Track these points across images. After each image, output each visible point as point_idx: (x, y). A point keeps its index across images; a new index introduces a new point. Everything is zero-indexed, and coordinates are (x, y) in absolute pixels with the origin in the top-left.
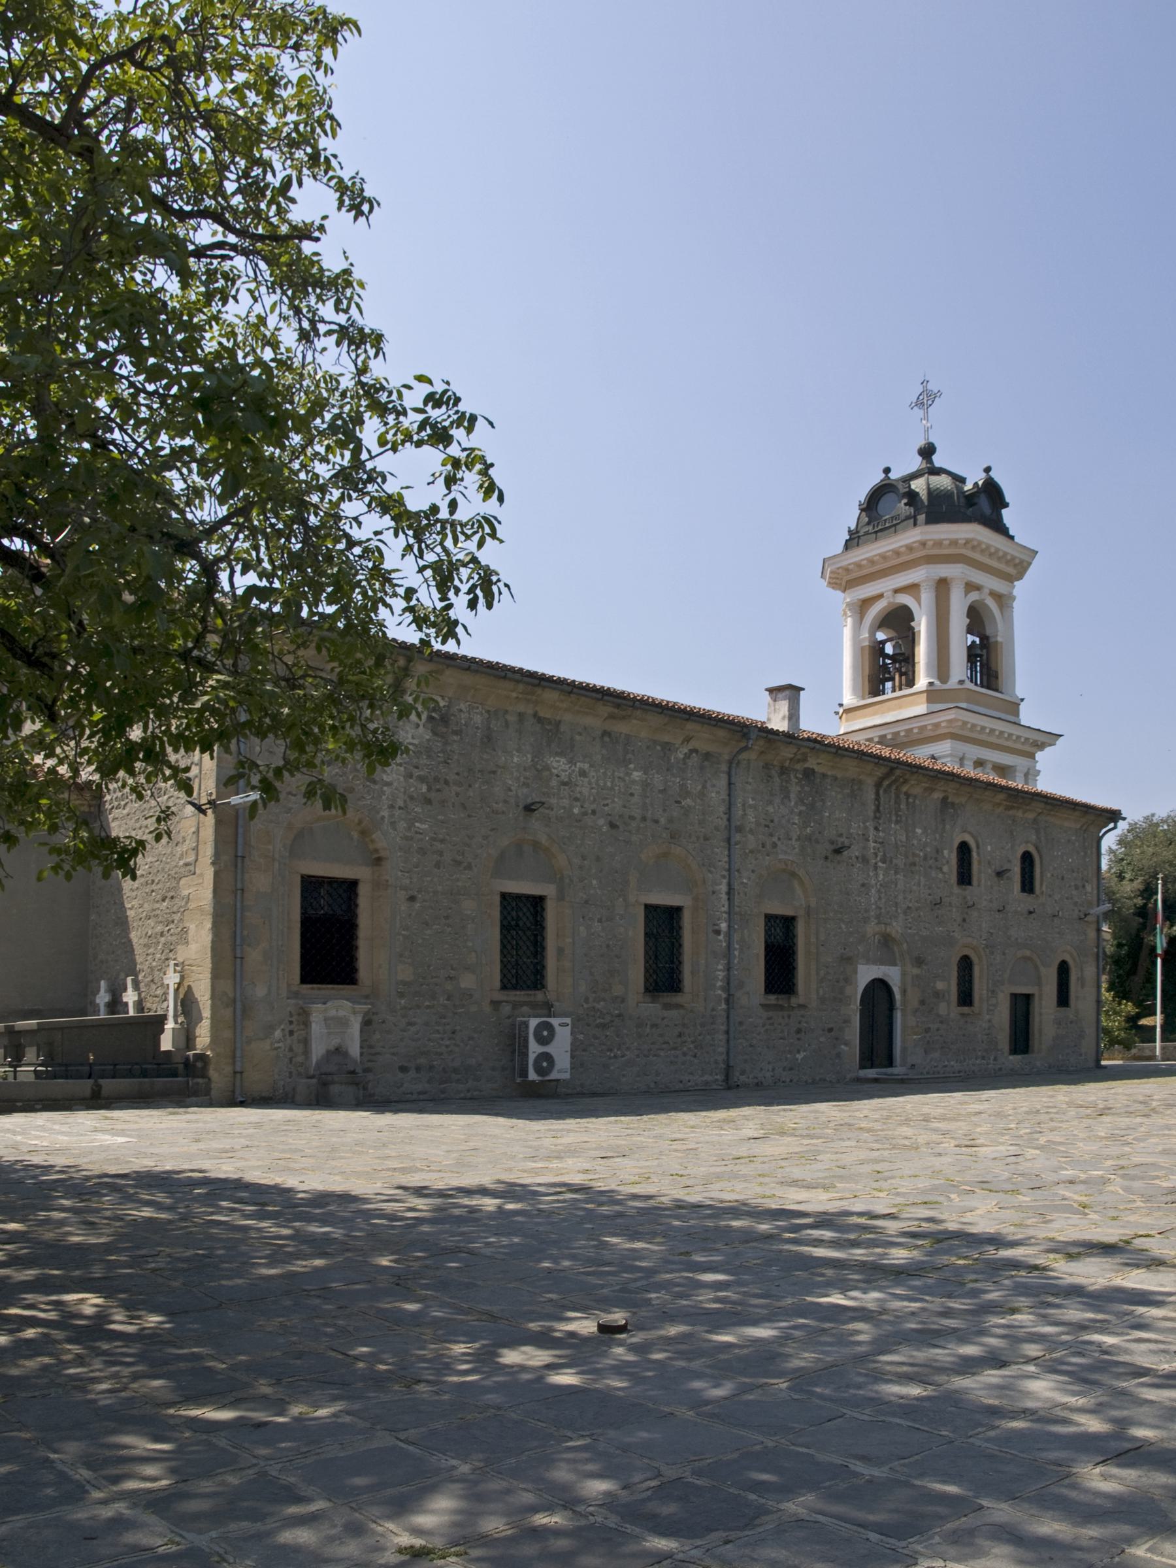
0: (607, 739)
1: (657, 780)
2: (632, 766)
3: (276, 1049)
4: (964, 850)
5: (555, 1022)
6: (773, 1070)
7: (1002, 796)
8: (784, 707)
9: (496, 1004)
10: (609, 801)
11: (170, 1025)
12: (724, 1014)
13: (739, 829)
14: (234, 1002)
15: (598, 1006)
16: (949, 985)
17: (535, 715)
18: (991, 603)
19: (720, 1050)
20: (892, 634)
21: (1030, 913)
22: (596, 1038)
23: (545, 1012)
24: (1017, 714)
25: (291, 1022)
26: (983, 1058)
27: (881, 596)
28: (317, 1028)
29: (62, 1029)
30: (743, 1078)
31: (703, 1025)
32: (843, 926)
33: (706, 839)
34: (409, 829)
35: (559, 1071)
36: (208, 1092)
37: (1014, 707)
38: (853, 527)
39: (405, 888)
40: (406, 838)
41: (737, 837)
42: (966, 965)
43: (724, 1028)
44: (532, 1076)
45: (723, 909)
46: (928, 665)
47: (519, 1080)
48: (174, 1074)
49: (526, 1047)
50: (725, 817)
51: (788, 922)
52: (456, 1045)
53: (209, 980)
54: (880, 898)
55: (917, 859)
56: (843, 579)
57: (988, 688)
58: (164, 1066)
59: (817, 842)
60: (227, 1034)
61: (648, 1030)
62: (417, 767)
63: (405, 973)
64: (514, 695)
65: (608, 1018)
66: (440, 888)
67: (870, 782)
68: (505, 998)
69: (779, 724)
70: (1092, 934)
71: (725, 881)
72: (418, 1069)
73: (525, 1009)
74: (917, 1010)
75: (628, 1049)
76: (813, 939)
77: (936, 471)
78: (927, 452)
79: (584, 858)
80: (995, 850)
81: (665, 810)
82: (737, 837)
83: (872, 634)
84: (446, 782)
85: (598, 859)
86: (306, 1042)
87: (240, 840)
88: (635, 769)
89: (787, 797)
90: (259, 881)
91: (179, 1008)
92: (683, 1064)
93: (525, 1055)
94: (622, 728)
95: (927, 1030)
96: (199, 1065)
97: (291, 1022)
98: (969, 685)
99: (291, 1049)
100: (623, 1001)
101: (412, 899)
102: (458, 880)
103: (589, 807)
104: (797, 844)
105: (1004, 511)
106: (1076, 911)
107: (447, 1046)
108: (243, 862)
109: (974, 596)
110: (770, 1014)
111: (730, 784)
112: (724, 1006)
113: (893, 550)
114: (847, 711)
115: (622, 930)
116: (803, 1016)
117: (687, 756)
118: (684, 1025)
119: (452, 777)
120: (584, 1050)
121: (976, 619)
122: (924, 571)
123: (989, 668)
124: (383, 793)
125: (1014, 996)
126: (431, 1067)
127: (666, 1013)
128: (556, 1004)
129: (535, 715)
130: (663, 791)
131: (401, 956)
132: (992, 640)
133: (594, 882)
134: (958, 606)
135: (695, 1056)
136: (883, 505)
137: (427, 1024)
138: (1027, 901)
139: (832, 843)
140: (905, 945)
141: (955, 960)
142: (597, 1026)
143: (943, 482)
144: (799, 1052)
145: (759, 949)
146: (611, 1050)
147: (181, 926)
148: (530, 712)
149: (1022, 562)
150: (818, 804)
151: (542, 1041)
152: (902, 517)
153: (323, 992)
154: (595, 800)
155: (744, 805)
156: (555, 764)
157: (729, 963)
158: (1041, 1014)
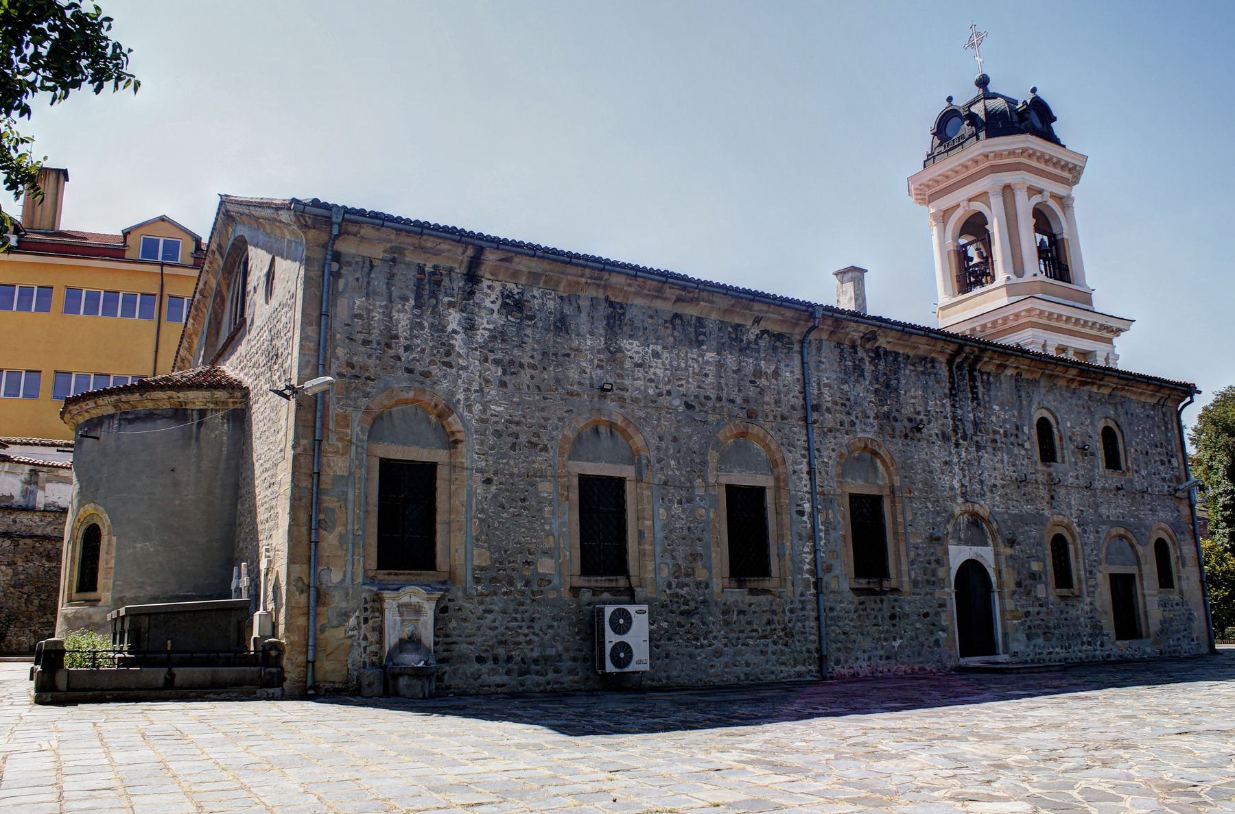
1: (731, 360)
2: (704, 347)
3: (351, 637)
4: (1044, 427)
5: (632, 609)
6: (869, 659)
8: (849, 288)
9: (575, 590)
10: (683, 382)
13: (816, 408)
14: (310, 591)
16: (1043, 564)
17: (607, 299)
19: (812, 638)
20: (972, 238)
25: (366, 609)
26: (1089, 644)
27: (958, 206)
28: (391, 616)
29: (149, 615)
31: (792, 611)
32: (930, 505)
33: (783, 418)
34: (484, 411)
37: (1086, 297)
40: (482, 421)
42: (1059, 545)
43: (814, 614)
45: (805, 489)
46: (1004, 261)
47: (600, 672)
50: (801, 396)
52: (534, 634)
54: (964, 476)
55: (997, 437)
59: (896, 419)
61: (735, 617)
62: (492, 351)
63: (482, 557)
64: (583, 280)
65: (693, 605)
66: (516, 471)
67: (942, 359)
68: (586, 584)
69: (847, 304)
70: (1185, 511)
71: (805, 460)
72: (496, 659)
73: (606, 596)
74: (1014, 593)
75: (715, 638)
76: (900, 519)
77: (995, 96)
78: (983, 82)
79: (661, 439)
81: (740, 390)
82: (815, 416)
83: (955, 240)
84: (521, 366)
86: (380, 630)
87: (318, 425)
88: (707, 350)
89: (862, 375)
90: (336, 465)
92: (774, 653)
94: (691, 311)
96: (273, 653)
97: (366, 609)
99: (365, 638)
100: (707, 586)
101: (488, 481)
104: (875, 423)
105: (1053, 125)
106: (1166, 488)
107: (526, 635)
108: (320, 445)
109: (1037, 199)
110: (862, 598)
111: (803, 363)
112: (813, 591)
113: (962, 165)
114: (943, 309)
115: (703, 511)
116: (896, 600)
117: (759, 337)
118: (774, 612)
119: (526, 360)
120: (669, 639)
121: (1042, 220)
122: (993, 178)
124: (459, 376)
125: (1114, 578)
126: (509, 659)
127: (753, 599)
128: (638, 590)
129: (607, 299)
131: (478, 540)
132: (1059, 237)
133: (672, 463)
134: (1024, 206)
135: (786, 645)
136: (949, 127)
137: (504, 612)
138: (1114, 479)
139: (910, 420)
140: (995, 524)
142: (682, 613)
143: (999, 104)
144: (895, 639)
146: (697, 639)
148: (601, 296)
149: (1075, 166)
150: (894, 382)
151: (619, 630)
153: (400, 577)
154: (669, 381)
155: (819, 384)
156: (629, 347)
157: (814, 546)
158: (1144, 595)
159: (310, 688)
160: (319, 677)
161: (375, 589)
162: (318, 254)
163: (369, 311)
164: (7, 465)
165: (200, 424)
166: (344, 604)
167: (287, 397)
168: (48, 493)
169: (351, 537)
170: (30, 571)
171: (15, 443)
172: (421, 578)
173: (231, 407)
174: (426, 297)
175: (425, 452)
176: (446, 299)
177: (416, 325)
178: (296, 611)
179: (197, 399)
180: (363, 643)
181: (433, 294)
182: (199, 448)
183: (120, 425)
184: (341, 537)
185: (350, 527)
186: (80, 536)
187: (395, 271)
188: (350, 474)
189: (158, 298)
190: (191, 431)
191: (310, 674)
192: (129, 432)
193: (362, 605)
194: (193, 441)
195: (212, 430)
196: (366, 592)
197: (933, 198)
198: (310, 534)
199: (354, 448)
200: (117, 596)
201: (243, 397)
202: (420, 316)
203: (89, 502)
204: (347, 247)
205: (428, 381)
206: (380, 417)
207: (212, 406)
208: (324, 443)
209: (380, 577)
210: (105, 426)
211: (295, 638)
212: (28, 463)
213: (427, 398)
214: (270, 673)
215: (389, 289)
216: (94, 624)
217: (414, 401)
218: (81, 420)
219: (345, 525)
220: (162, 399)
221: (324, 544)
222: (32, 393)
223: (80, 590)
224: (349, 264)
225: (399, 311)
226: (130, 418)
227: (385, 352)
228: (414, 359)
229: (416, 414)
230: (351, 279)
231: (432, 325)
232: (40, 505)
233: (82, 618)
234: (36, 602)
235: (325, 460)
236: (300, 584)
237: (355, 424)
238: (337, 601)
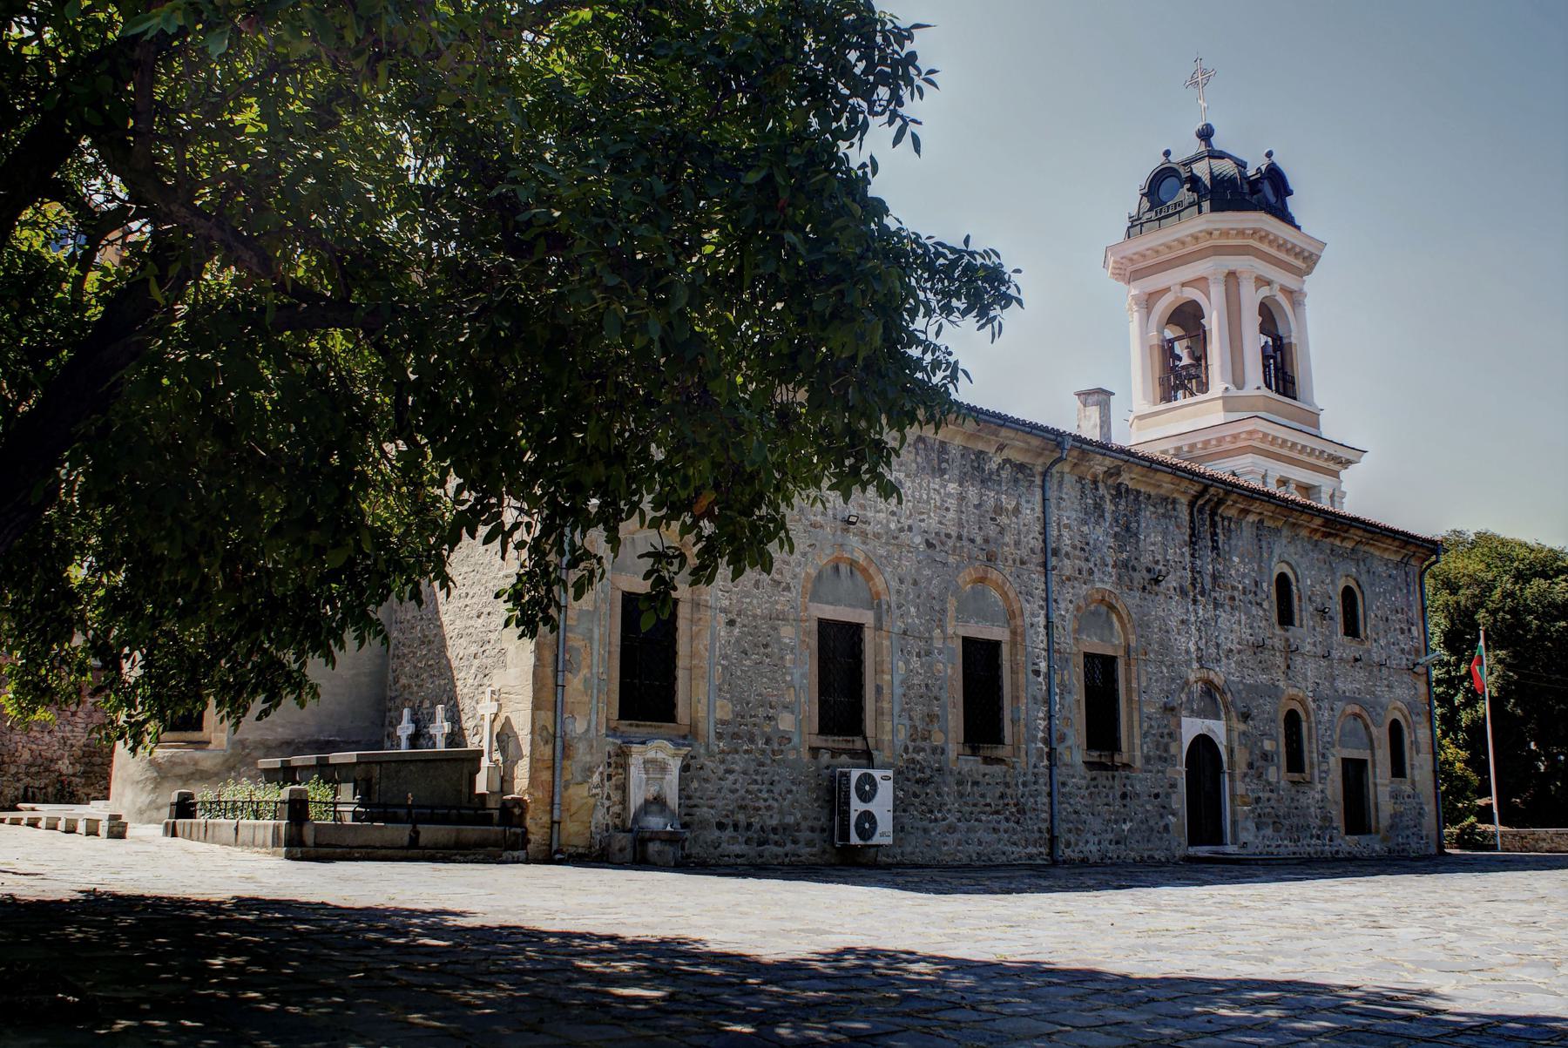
0: (921, 446)
1: (972, 493)
4: (1283, 583)
7: (1318, 521)
8: (1094, 413)
9: (815, 751)
11: (485, 762)
12: (1047, 771)
14: (555, 743)
15: (919, 757)
16: (1275, 744)
18: (1281, 298)
19: (1044, 815)
21: (1356, 660)
22: (916, 795)
23: (864, 762)
24: (1316, 425)
25: (609, 765)
26: (1318, 837)
27: (1168, 289)
28: (636, 773)
29: (380, 763)
30: (1068, 852)
31: (1025, 784)
33: (1023, 563)
35: (882, 835)
36: (521, 842)
38: (1134, 213)
39: (724, 611)
41: (1053, 561)
42: (1292, 720)
44: (855, 840)
48: (487, 820)
49: (848, 804)
50: (1040, 538)
51: (1108, 663)
53: (529, 712)
56: (1132, 271)
57: (1285, 394)
58: (472, 809)
59: (1134, 569)
60: (546, 776)
65: (928, 772)
66: (759, 611)
69: (1091, 432)
73: (844, 758)
76: (1134, 685)
78: (1206, 134)
79: (901, 581)
80: (1318, 582)
82: (1053, 561)
83: (1161, 331)
85: (915, 583)
86: (623, 788)
91: (495, 744)
93: (845, 814)
95: (1258, 800)
96: (517, 811)
98: (1265, 391)
99: (609, 797)
101: (731, 623)
102: (777, 602)
103: (906, 523)
109: (1265, 291)
112: (1046, 762)
114: (1140, 418)
115: (940, 667)
117: (1001, 467)
118: (1007, 785)
121: (1269, 318)
122: (1210, 258)
123: (1285, 373)
126: (749, 826)
130: (977, 507)
132: (1285, 341)
134: (1251, 298)
136: (1165, 189)
137: (745, 773)
139: (1149, 570)
141: (1281, 716)
142: (917, 782)
143: (1226, 168)
145: (1078, 694)
146: (931, 812)
147: (498, 647)
150: (1134, 525)
152: (1186, 203)
153: (641, 729)
157: (1049, 711)
158: (1375, 785)
160: (563, 841)
161: (619, 742)
166: (588, 758)
180: (607, 803)
185: (595, 670)
196: (611, 744)
197: (1136, 276)
198: (556, 676)
209: (622, 728)
211: (539, 794)
219: (590, 667)
233: (183, 764)
238: (582, 754)
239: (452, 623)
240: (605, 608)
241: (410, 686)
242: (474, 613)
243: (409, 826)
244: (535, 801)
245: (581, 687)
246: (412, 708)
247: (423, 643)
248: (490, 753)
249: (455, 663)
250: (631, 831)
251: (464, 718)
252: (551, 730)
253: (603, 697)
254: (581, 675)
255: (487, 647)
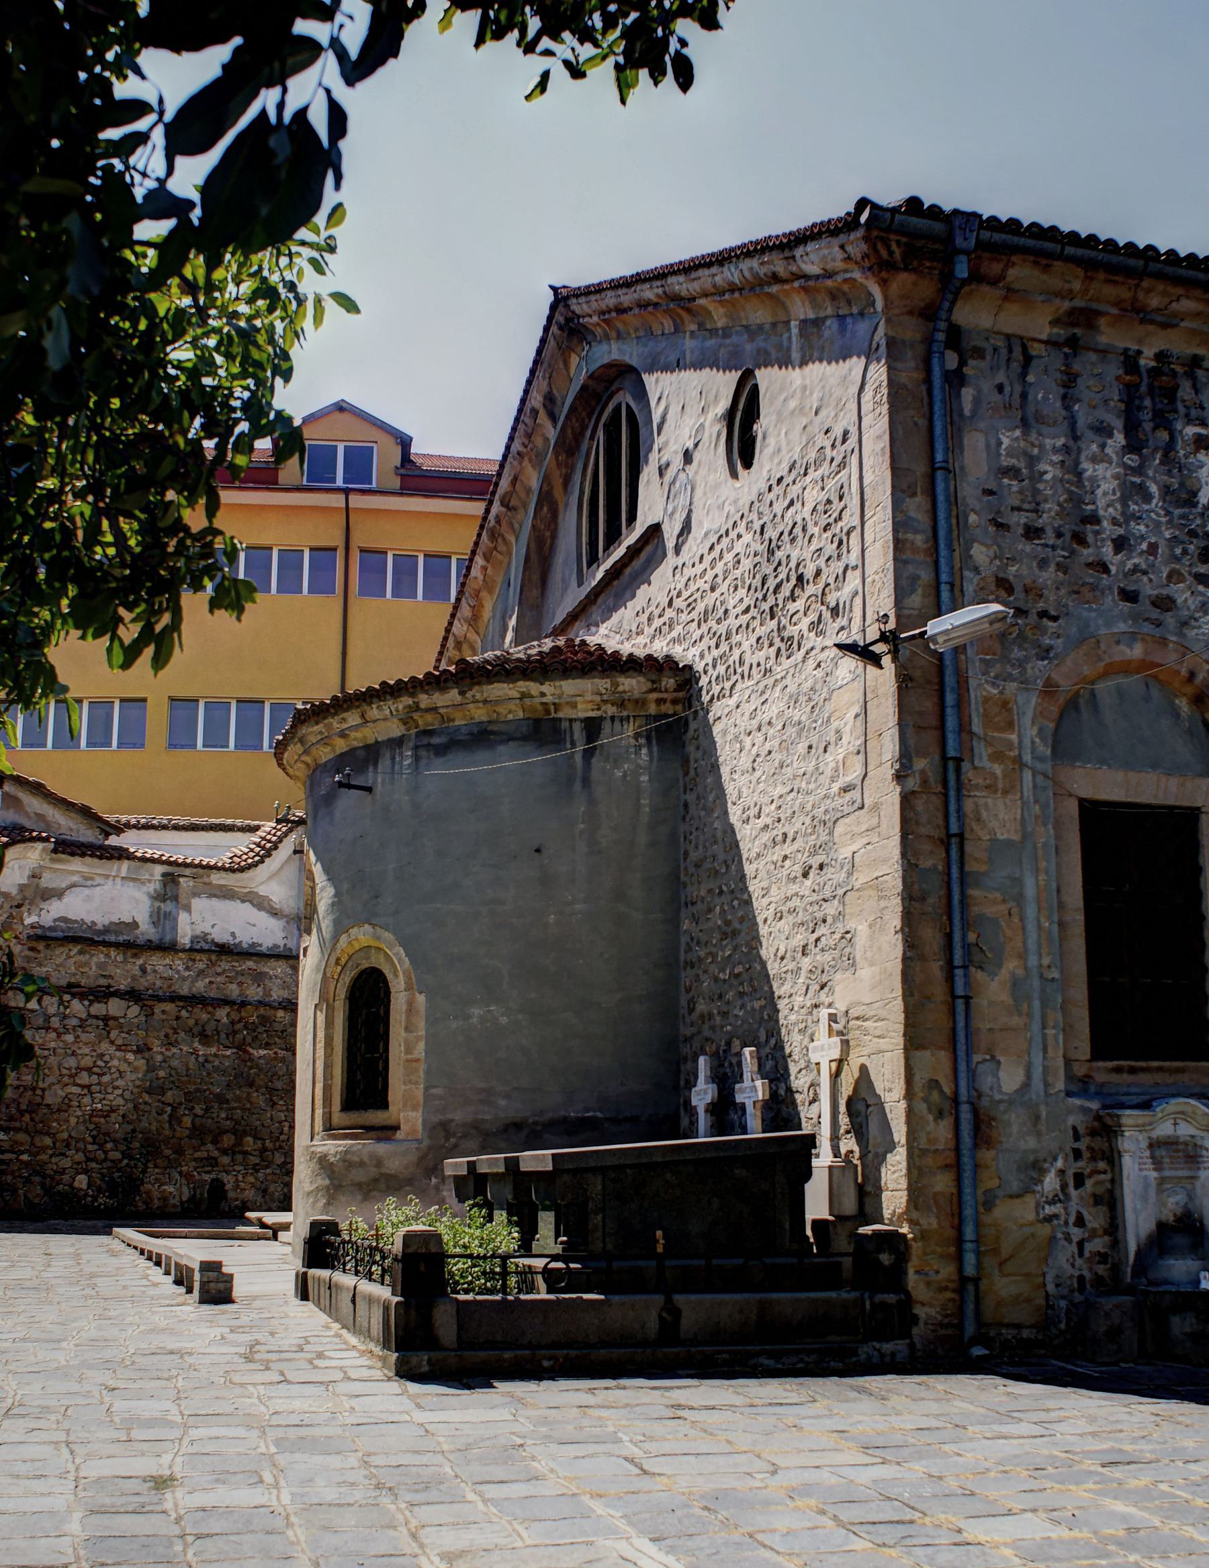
3: (1049, 1219)
11: (823, 1159)
14: (959, 1118)
25: (1077, 1154)
29: (602, 1170)
36: (902, 1317)
53: (899, 1054)
60: (942, 1183)
86: (1110, 1201)
87: (951, 722)
90: (997, 816)
91: (844, 1120)
96: (885, 1258)
99: (1080, 1222)
108: (958, 771)
147: (840, 928)
153: (1142, 1078)
159: (974, 1341)
160: (988, 1315)
161: (1094, 1105)
162: (912, 331)
163: (1032, 461)
164: (125, 865)
165: (588, 754)
166: (1031, 1143)
167: (875, 660)
168: (196, 916)
169: (1036, 983)
170: (175, 1063)
171: (128, 826)
172: (1185, 1078)
173: (652, 709)
174: (1148, 426)
175: (1173, 783)
176: (1191, 431)
177: (1132, 491)
178: (929, 1160)
179: (579, 696)
180: (1077, 1233)
181: (1162, 420)
182: (592, 802)
183: (417, 758)
184: (1016, 984)
185: (1033, 961)
186: (342, 993)
187: (1076, 367)
188: (1025, 836)
189: (340, 555)
190: (572, 766)
191: (970, 1308)
192: (439, 771)
193: (1070, 1144)
194: (578, 786)
195: (617, 764)
196: (1077, 1112)
198: (950, 979)
199: (1028, 776)
200: (436, 1118)
201: (679, 688)
202: (1139, 470)
203: (359, 923)
204: (976, 314)
205: (1169, 619)
206: (1072, 704)
207: (611, 710)
208: (966, 766)
209: (1100, 1078)
210: (384, 763)
211: (931, 1222)
212: (158, 861)
213: (1169, 658)
214: (883, 1304)
215: (1067, 408)
216: (389, 1178)
217: (1144, 665)
218: (325, 754)
219: (1023, 956)
220: (507, 699)
221: (981, 1003)
222: (133, 738)
223: (347, 1106)
224: (979, 353)
225: (1094, 460)
226: (438, 742)
227: (1073, 552)
228: (1136, 569)
229: (1147, 699)
230: (987, 386)
231: (1166, 490)
232: (185, 940)
233: (362, 1164)
234: (187, 1121)
235: (968, 805)
236: (935, 1096)
237: (1027, 720)
238: (1016, 1137)
239: (766, 892)
240: (1044, 835)
241: (710, 1016)
242: (798, 869)
243: (659, 1299)
244: (923, 1236)
245: (1005, 997)
246: (715, 1055)
247: (724, 936)
248: (835, 1139)
249: (773, 968)
250: (1130, 1290)
251: (793, 1069)
252: (948, 1090)
253: (1056, 1016)
254: (1004, 974)
255: (822, 930)
